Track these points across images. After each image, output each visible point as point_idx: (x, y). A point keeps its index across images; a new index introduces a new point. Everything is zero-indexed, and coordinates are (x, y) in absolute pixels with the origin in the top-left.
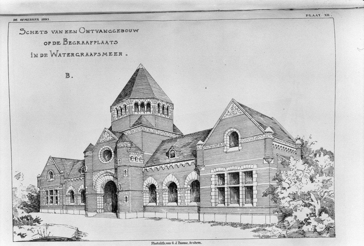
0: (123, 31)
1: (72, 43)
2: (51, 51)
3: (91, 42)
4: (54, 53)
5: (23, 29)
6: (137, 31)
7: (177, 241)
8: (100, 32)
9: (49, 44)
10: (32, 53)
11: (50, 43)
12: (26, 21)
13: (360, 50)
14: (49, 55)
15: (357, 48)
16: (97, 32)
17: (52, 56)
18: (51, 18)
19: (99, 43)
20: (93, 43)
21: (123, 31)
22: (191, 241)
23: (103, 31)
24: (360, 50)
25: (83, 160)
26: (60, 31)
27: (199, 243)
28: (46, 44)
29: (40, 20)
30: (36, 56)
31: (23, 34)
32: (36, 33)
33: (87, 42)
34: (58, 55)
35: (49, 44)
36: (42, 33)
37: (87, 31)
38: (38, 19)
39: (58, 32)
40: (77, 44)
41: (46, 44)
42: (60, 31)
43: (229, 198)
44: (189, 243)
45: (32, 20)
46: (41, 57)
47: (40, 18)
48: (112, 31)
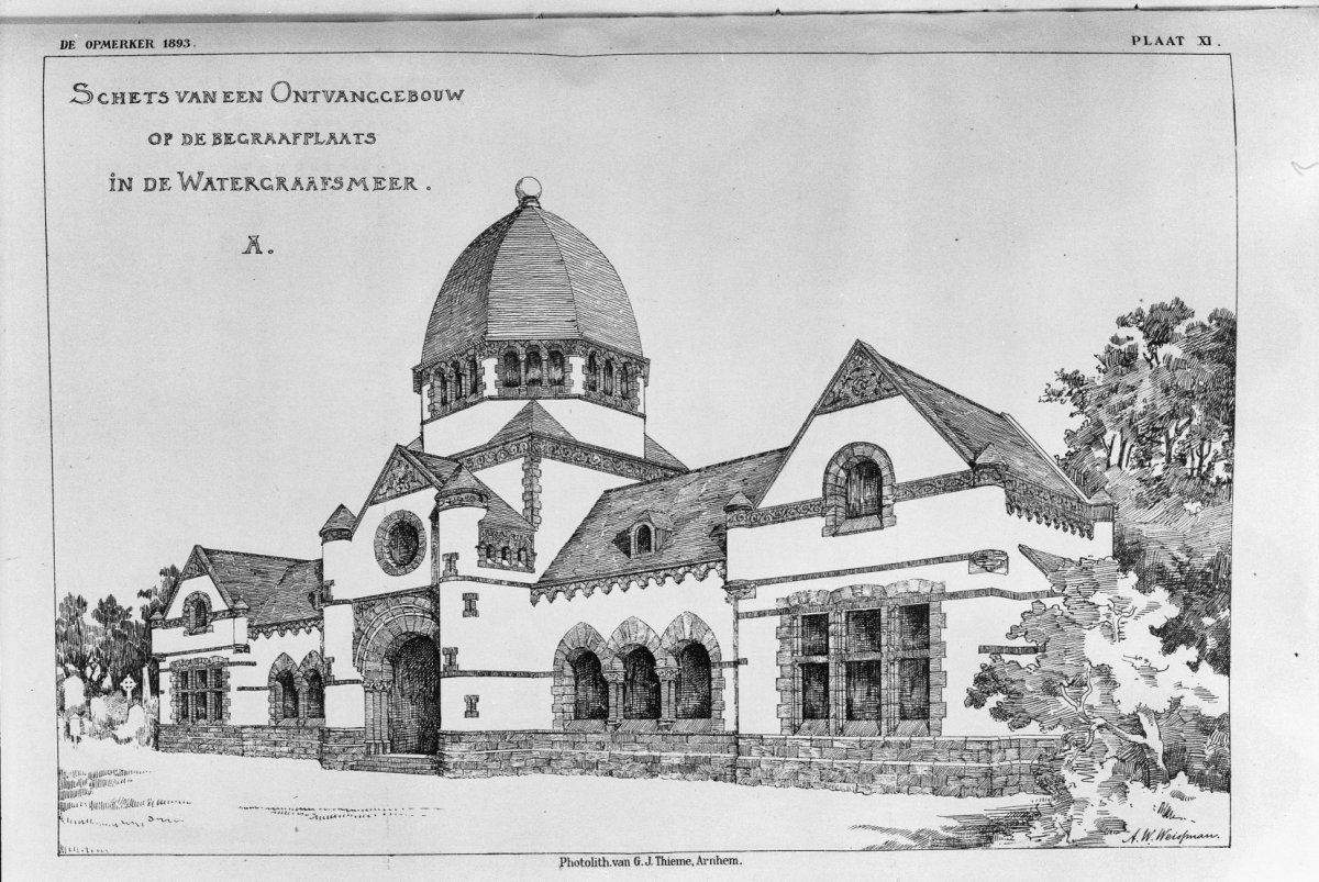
0: (413, 96)
1: (234, 138)
2: (181, 174)
3: (296, 136)
4: (190, 179)
5: (85, 85)
6: (458, 96)
7: (653, 856)
8: (190, 101)
9: (167, 144)
10: (113, 174)
11: (169, 136)
12: (106, 51)
13: (1300, 170)
14: (175, 182)
15: (1293, 163)
16: (181, 101)
17: (185, 187)
18: (201, 37)
19: (1149, 40)
20: (301, 140)
21: (413, 96)
22: (703, 856)
23: (349, 96)
24: (1300, 170)
25: (317, 561)
26: (354, 94)
27: (734, 861)
28: (155, 139)
29: (158, 44)
30: (126, 185)
31: (273, 90)
32: (132, 102)
33: (284, 137)
34: (204, 182)
35: (167, 144)
36: (150, 102)
37: (297, 93)
38: (150, 44)
39: (349, 96)
40: (250, 142)
41: (155, 139)
42: (354, 94)
43: (858, 738)
44: (695, 861)
45: (128, 45)
46: (146, 189)
47: (160, 34)
48: (378, 96)
